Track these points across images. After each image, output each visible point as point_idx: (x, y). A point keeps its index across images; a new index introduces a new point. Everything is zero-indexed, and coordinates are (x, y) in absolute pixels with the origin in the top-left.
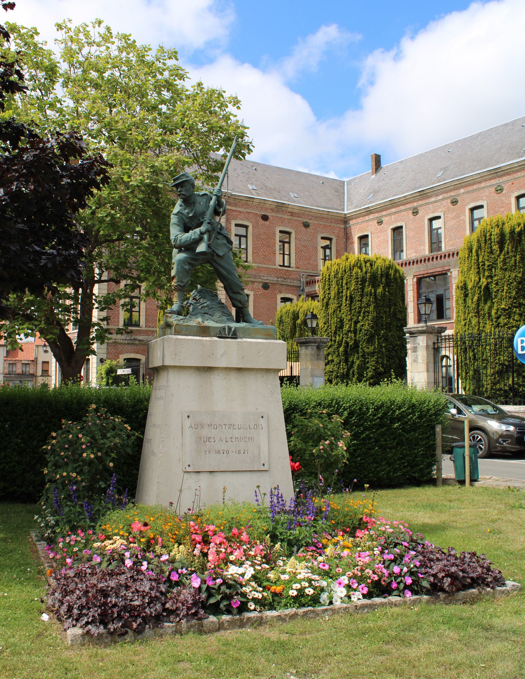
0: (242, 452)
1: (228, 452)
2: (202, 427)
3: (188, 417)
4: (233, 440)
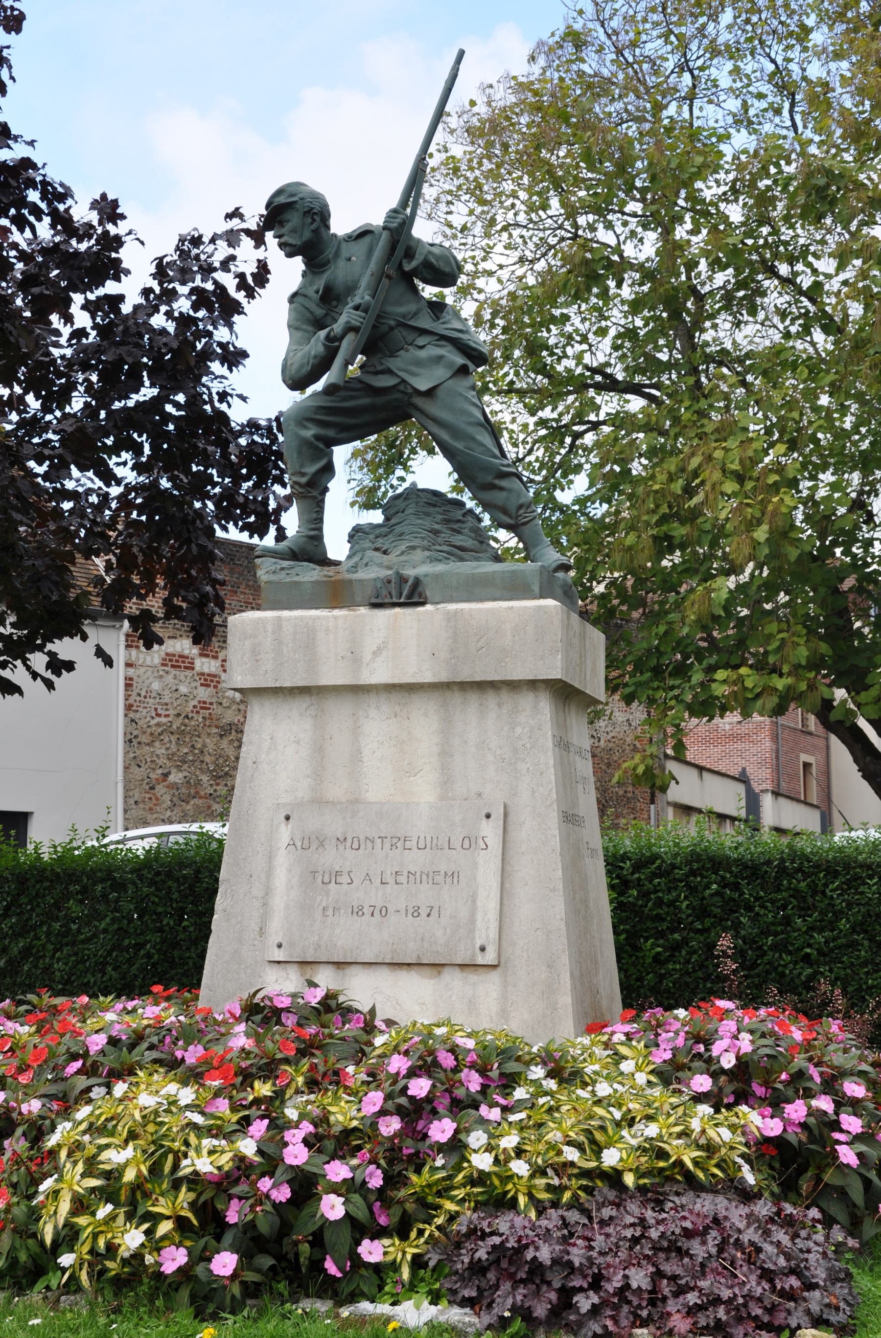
0: (424, 912)
1: (384, 912)
2: (322, 844)
3: (288, 818)
4: (402, 879)
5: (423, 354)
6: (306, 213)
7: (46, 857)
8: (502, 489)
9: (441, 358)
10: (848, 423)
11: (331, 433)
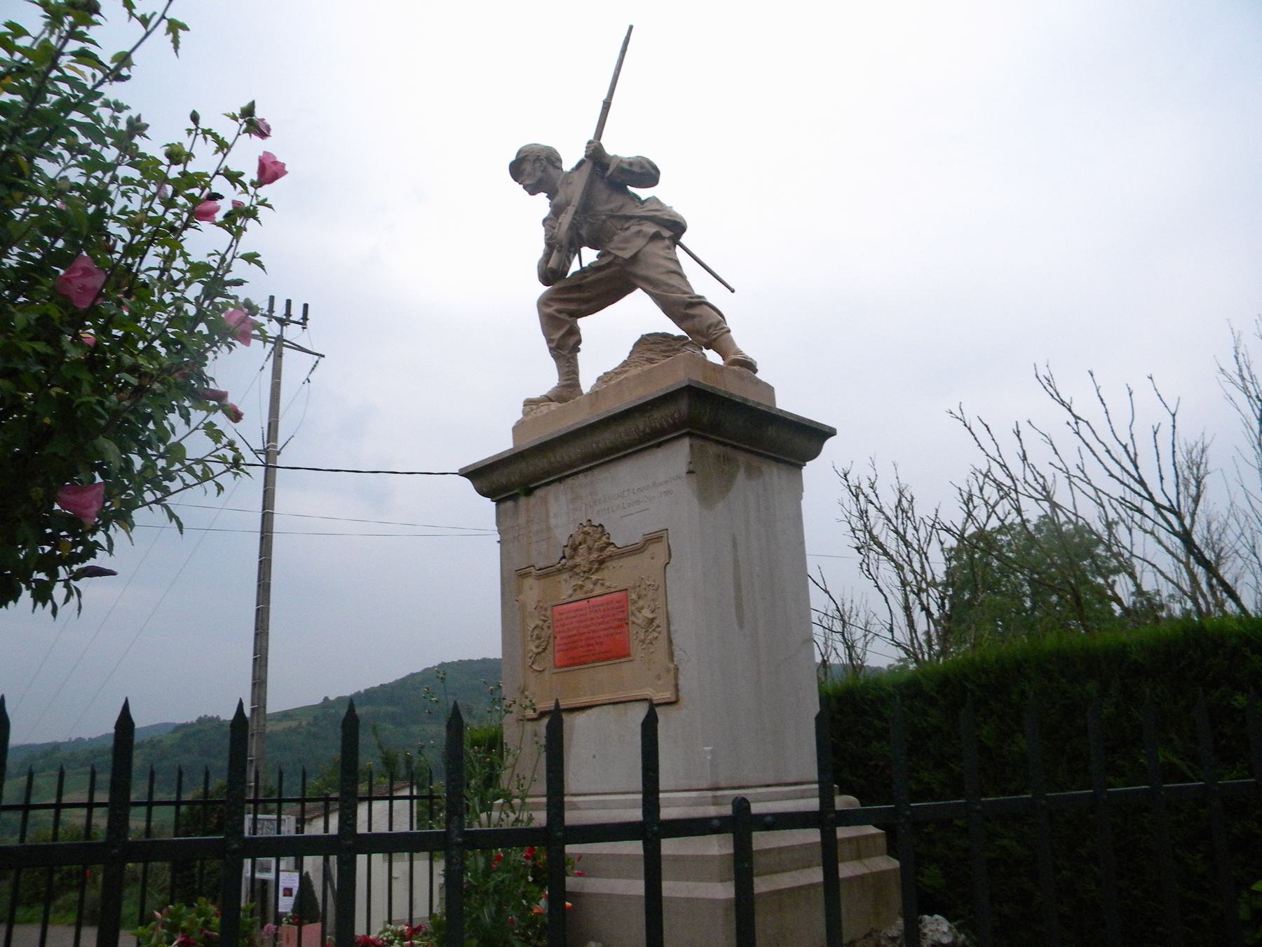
5: (628, 233)
6: (534, 162)
7: (775, 473)
8: (693, 317)
9: (640, 231)
10: (546, 875)
11: (572, 307)
